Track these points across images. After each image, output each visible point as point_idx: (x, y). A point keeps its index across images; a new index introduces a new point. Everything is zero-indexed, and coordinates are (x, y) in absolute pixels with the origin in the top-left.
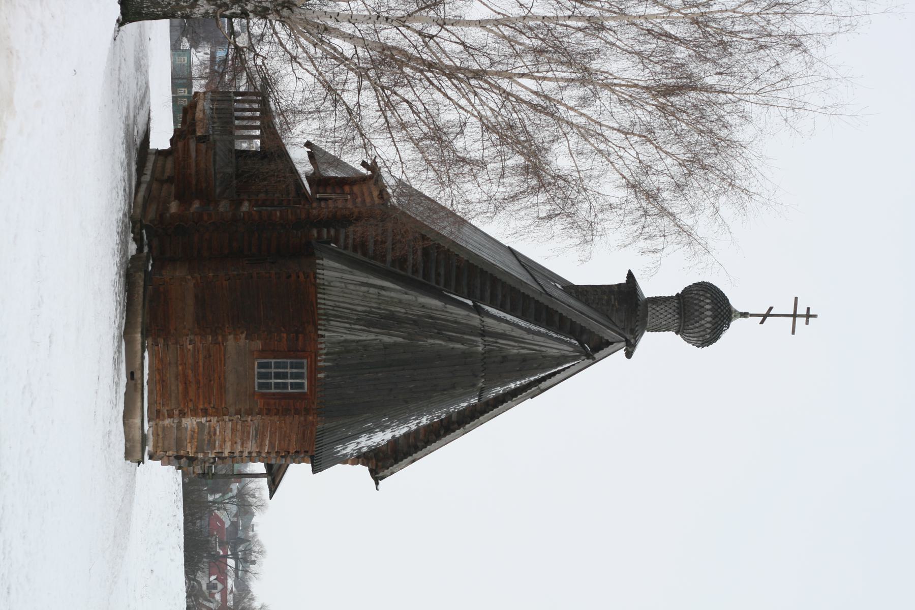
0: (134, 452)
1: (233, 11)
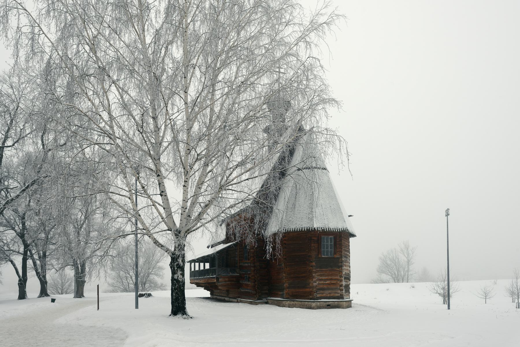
0: (349, 305)
1: (181, 261)
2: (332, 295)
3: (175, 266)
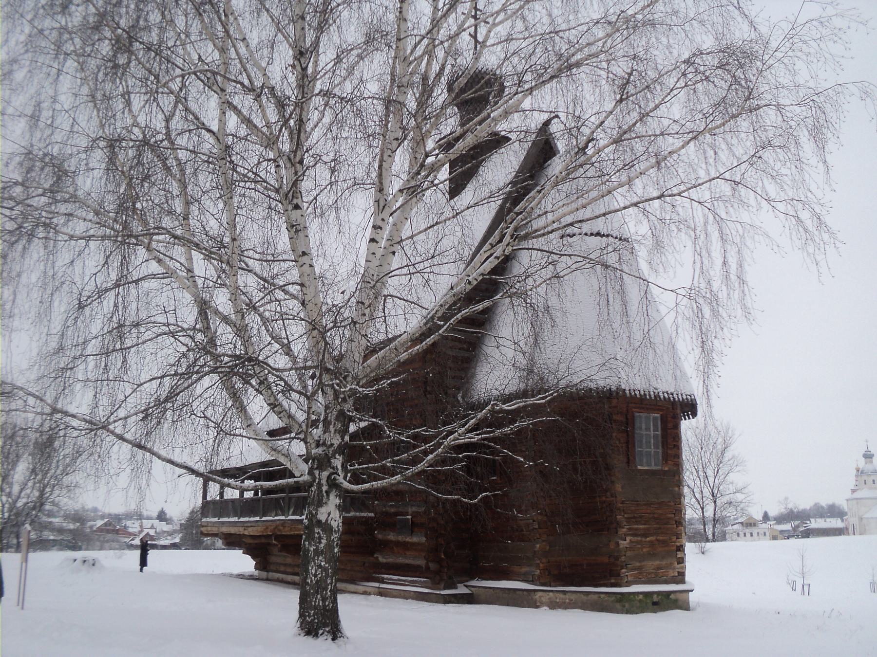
1: (339, 467)
3: (324, 482)
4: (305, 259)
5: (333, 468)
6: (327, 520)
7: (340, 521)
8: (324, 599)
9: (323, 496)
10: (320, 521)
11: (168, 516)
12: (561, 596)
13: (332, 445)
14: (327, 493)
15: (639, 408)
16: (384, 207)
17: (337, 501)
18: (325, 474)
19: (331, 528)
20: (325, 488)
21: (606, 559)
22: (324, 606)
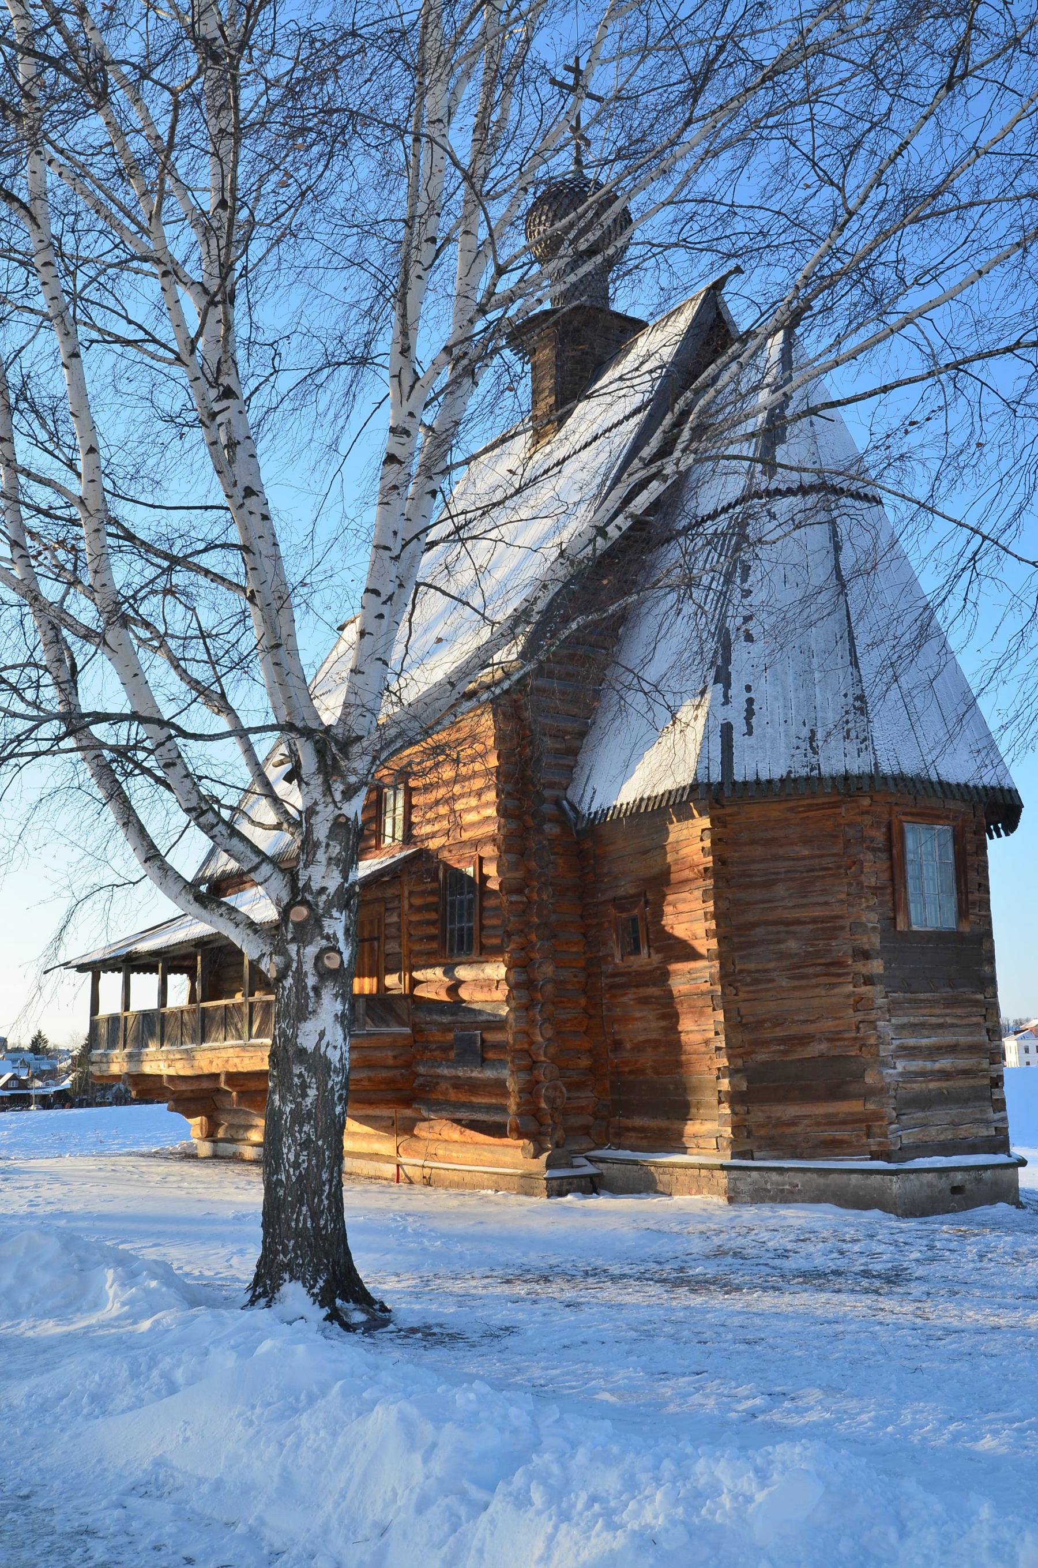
1: (341, 935)
2: (964, 1131)
3: (308, 967)
4: (252, 503)
5: (328, 938)
6: (317, 1047)
7: (345, 1048)
8: (315, 1215)
9: (308, 997)
10: (303, 1051)
11: (50, 1045)
12: (775, 1177)
13: (323, 890)
14: (316, 990)
15: (912, 814)
16: (412, 387)
17: (338, 1007)
18: (311, 951)
19: (328, 1063)
20: (311, 981)
21: (517, 1062)
22: (317, 1229)
